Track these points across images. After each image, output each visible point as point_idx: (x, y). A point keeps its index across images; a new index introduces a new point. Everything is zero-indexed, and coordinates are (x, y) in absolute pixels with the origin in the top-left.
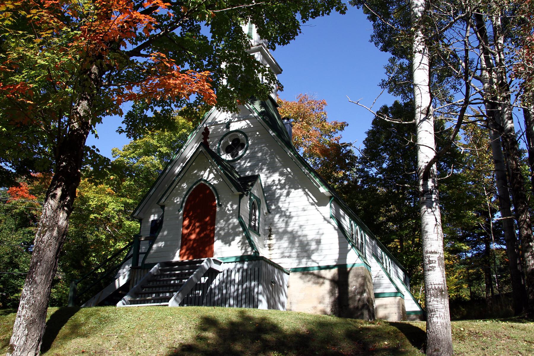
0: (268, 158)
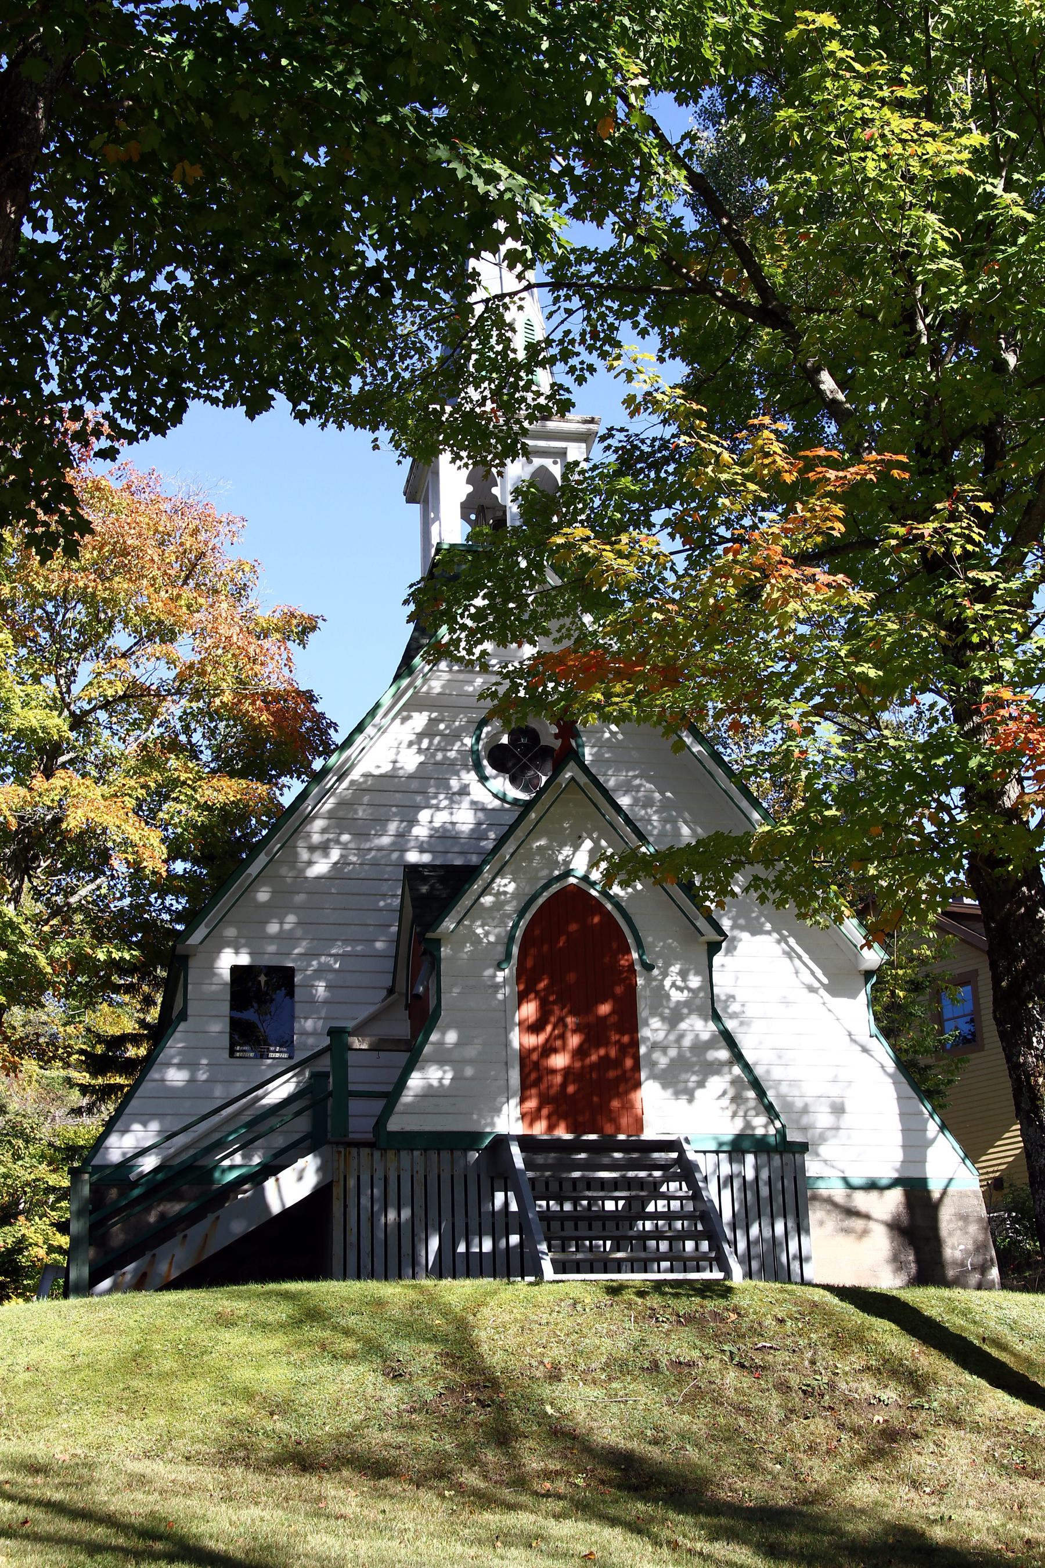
0: (655, 818)
